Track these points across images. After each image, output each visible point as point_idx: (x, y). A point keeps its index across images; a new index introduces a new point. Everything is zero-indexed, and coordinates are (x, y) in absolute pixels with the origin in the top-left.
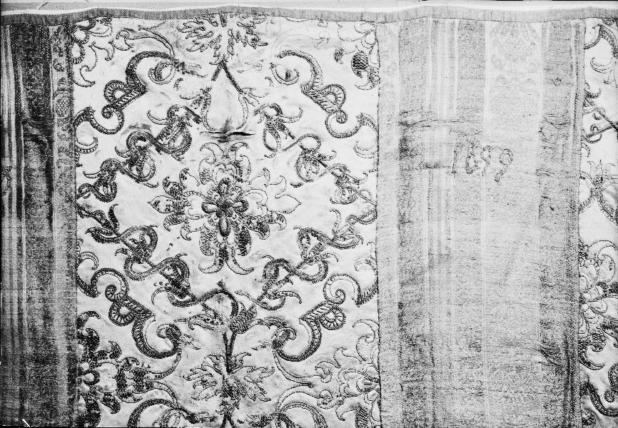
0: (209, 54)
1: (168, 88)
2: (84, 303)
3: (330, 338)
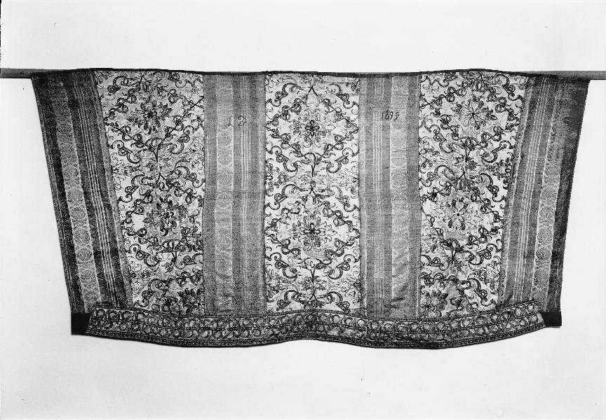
0: (308, 85)
1: (295, 94)
2: (268, 156)
3: (280, 89)
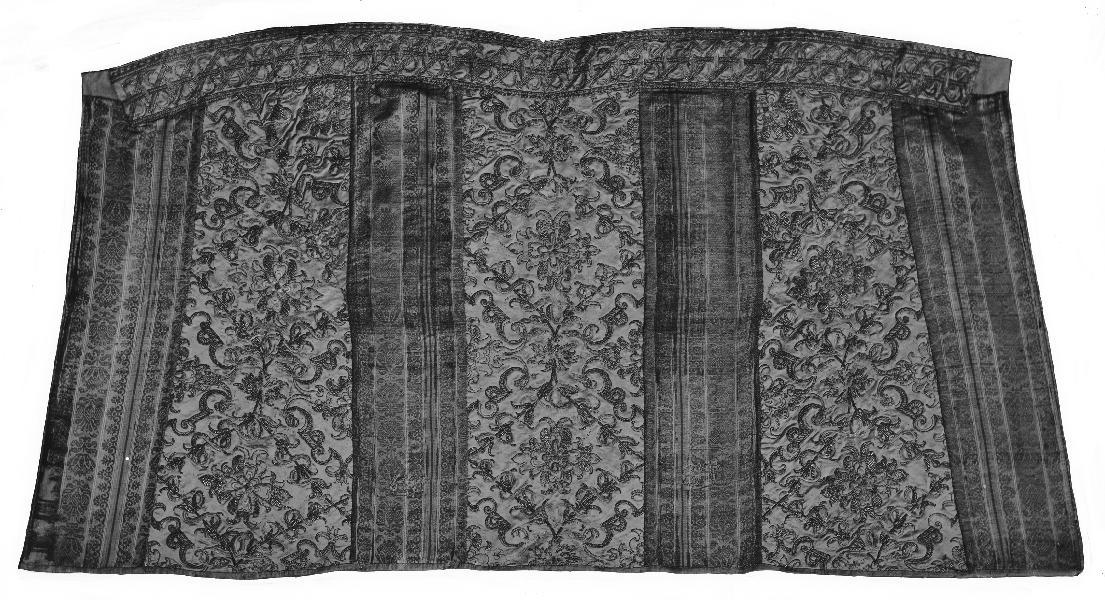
3: (495, 381)
